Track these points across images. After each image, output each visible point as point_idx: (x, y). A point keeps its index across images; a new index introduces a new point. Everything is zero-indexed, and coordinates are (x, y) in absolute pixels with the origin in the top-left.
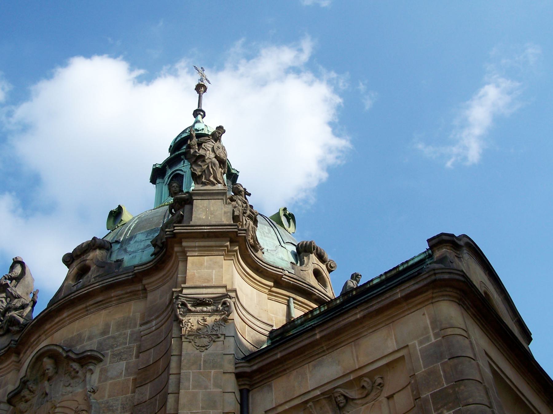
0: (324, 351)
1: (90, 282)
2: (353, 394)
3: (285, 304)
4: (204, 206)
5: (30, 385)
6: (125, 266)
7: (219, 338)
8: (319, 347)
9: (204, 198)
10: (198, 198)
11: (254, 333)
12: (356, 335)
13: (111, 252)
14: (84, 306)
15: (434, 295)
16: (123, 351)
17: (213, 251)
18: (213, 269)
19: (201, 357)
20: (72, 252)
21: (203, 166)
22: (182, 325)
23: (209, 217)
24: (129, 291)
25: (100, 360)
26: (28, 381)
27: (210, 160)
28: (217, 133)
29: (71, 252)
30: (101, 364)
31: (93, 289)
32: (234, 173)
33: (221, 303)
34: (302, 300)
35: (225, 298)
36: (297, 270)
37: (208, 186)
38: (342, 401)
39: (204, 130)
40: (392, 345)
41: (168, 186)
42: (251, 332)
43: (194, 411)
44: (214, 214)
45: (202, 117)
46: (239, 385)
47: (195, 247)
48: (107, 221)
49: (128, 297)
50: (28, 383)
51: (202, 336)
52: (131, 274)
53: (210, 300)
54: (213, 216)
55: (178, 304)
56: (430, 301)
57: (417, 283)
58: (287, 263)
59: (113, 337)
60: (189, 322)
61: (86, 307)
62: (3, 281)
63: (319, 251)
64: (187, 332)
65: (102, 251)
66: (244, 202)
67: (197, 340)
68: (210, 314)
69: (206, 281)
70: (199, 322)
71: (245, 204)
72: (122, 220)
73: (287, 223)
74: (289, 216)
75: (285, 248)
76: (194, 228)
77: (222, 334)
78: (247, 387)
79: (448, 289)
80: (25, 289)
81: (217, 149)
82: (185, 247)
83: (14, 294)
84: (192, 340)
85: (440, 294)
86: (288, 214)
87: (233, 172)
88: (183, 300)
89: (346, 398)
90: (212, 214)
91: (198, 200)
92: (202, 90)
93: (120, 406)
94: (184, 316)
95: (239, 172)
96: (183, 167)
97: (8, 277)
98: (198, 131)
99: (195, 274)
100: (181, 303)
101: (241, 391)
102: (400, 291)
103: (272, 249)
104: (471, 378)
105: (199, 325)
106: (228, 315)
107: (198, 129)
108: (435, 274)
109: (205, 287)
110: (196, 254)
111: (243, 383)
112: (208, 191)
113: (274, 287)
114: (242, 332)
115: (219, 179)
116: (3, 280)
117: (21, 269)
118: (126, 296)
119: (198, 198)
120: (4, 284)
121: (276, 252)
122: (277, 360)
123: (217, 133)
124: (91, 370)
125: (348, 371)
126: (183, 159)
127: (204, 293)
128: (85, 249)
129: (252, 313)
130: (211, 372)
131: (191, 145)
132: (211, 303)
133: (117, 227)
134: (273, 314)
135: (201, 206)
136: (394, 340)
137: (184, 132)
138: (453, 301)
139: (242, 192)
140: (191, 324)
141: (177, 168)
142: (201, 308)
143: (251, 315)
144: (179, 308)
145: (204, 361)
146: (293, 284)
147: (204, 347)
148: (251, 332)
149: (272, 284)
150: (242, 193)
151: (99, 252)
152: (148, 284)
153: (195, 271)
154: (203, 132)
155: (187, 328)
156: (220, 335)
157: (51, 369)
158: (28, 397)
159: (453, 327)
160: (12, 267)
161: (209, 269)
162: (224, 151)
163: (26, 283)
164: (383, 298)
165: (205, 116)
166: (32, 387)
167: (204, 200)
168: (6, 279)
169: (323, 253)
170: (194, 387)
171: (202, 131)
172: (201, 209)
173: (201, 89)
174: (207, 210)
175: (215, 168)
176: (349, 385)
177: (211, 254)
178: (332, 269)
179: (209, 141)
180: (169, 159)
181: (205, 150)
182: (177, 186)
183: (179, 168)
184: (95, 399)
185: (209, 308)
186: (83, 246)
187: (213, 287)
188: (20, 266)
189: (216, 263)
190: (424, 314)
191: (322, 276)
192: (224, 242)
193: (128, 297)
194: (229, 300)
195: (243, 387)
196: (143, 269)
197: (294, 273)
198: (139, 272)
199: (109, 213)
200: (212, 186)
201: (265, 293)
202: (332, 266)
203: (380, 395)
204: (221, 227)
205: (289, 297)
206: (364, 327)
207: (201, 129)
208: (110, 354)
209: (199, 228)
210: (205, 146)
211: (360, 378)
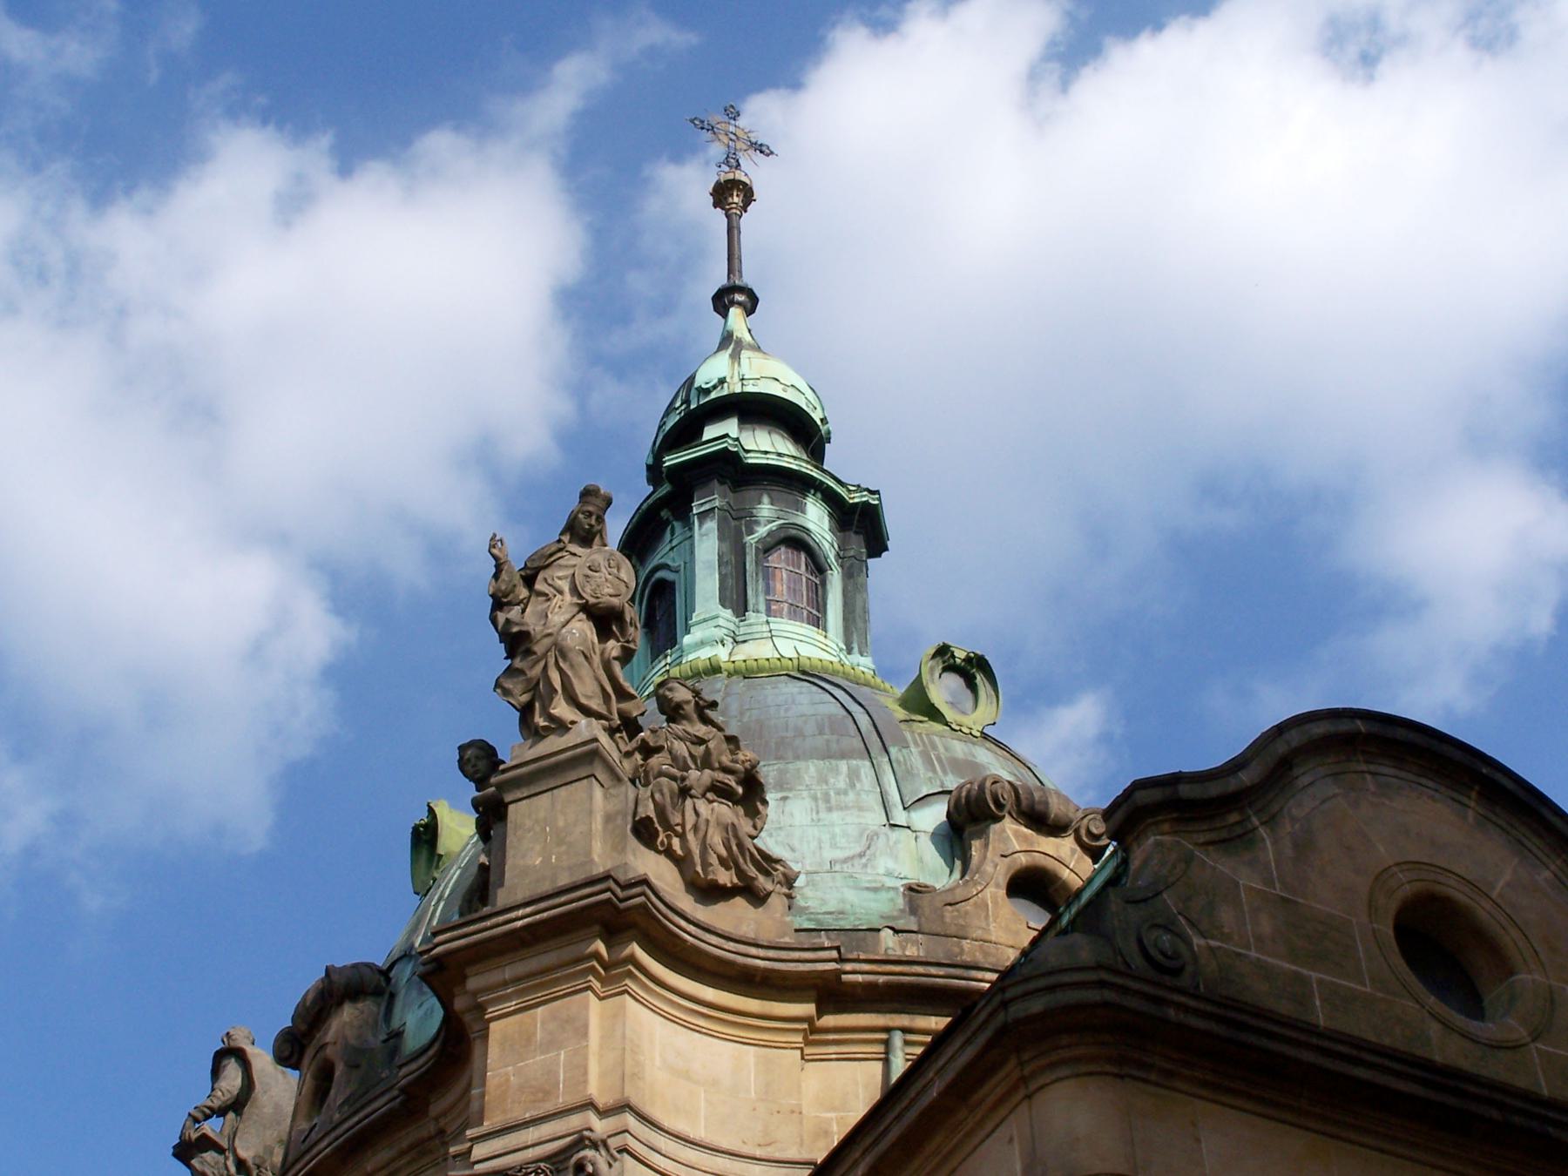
4: (537, 821)
6: (407, 1053)
9: (540, 790)
10: (519, 795)
13: (392, 996)
15: (1027, 1071)
17: (557, 982)
20: (292, 1022)
21: (528, 672)
23: (554, 857)
24: (405, 1144)
27: (547, 641)
28: (581, 516)
29: (290, 1025)
31: (316, 1159)
35: (578, 1152)
36: (927, 911)
39: (728, 380)
41: (644, 630)
44: (568, 839)
47: (505, 984)
48: (412, 864)
49: (409, 1163)
53: (540, 1168)
54: (564, 848)
56: (1022, 1092)
57: (968, 1042)
58: (891, 894)
63: (1024, 803)
65: (360, 1005)
66: (694, 739)
69: (540, 1095)
74: (969, 668)
75: (909, 827)
76: (488, 923)
79: (1065, 1040)
80: (268, 1133)
82: (475, 993)
85: (1043, 1062)
87: (856, 500)
90: (560, 842)
91: (520, 803)
95: (877, 492)
96: (671, 552)
98: (707, 392)
99: (508, 1080)
102: (936, 1074)
103: (847, 853)
107: (704, 386)
108: (1005, 1005)
110: (512, 1005)
112: (553, 760)
113: (821, 1012)
116: (190, 1128)
117: (240, 1074)
118: (402, 1162)
119: (519, 795)
121: (864, 860)
123: (581, 516)
126: (667, 522)
128: (316, 1010)
129: (725, 1145)
134: (834, 1109)
135: (528, 823)
137: (670, 409)
138: (1091, 1074)
143: (723, 1152)
146: (887, 985)
150: (683, 709)
151: (351, 1011)
152: (444, 1114)
153: (510, 1068)
154: (725, 392)
160: (216, 1072)
161: (548, 1052)
162: (618, 570)
163: (268, 1110)
164: (903, 1105)
168: (196, 1120)
169: (1040, 802)
171: (719, 388)
172: (529, 831)
173: (730, 200)
174: (548, 829)
175: (568, 663)
177: (552, 996)
178: (1098, 844)
179: (559, 555)
180: (629, 532)
181: (547, 595)
182: (477, 757)
183: (660, 561)
186: (308, 1004)
187: (554, 1114)
189: (567, 1021)
191: (1059, 883)
193: (409, 1163)
197: (915, 928)
198: (410, 1084)
199: (410, 836)
201: (792, 1048)
205: (888, 1030)
207: (715, 381)
209: (501, 919)
210: (545, 580)
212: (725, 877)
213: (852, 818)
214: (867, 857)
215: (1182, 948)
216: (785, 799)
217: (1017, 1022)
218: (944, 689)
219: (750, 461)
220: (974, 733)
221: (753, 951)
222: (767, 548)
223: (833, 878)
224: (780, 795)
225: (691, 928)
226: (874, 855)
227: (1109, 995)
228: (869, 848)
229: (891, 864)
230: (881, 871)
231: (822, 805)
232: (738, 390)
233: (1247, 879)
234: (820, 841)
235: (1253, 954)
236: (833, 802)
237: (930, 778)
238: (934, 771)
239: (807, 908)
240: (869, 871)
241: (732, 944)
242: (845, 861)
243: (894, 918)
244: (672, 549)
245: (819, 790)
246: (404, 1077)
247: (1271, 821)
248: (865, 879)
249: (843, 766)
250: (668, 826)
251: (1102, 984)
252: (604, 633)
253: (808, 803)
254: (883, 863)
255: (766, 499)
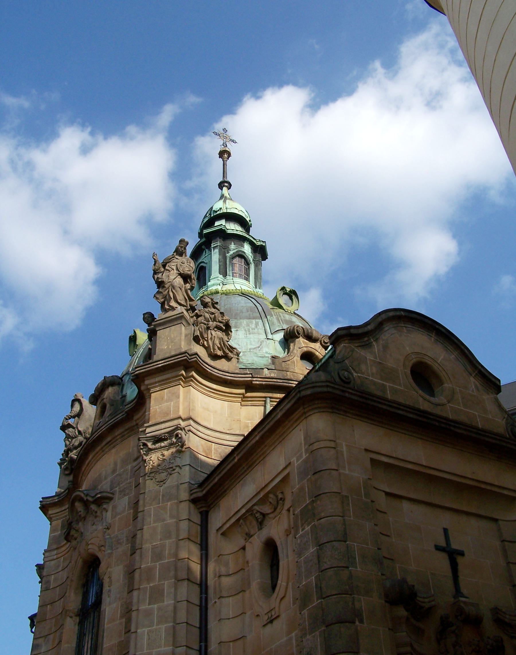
0: (246, 471)
1: (105, 420)
2: (266, 509)
3: (263, 406)
5: (74, 525)
7: (174, 470)
8: (241, 468)
9: (166, 327)
11: (223, 449)
12: (263, 454)
14: (99, 448)
15: (306, 410)
16: (125, 486)
18: (172, 401)
19: (160, 492)
20: (95, 392)
22: (146, 464)
25: (111, 499)
26: (72, 522)
27: (169, 284)
28: (179, 248)
30: (112, 502)
32: (259, 245)
33: (174, 436)
34: (279, 396)
37: (170, 312)
38: (259, 517)
39: (222, 208)
40: (282, 464)
42: (219, 448)
43: (154, 544)
45: (228, 188)
46: (199, 509)
47: (156, 383)
50: (73, 524)
51: (161, 471)
52: (124, 413)
54: (173, 344)
55: (140, 446)
57: (289, 402)
58: (267, 358)
59: (120, 475)
60: (150, 460)
61: (102, 448)
62: (65, 422)
63: (306, 333)
64: (150, 470)
65: (114, 388)
67: (157, 476)
68: (167, 448)
69: (166, 415)
70: (159, 458)
71: (213, 314)
72: (137, 345)
73: (290, 300)
75: (272, 339)
77: (176, 466)
78: (204, 509)
81: (181, 265)
82: (148, 385)
83: (71, 435)
84: (153, 477)
85: (310, 408)
86: (289, 291)
87: (259, 244)
88: (143, 441)
89: (262, 514)
90: (172, 342)
92: (226, 156)
93: (125, 538)
94: (147, 455)
97: (69, 417)
98: (216, 212)
100: (142, 444)
101: (201, 513)
103: (255, 347)
104: (327, 491)
105: (159, 461)
106: (182, 446)
107: (215, 210)
109: (164, 422)
110: (158, 389)
111: (200, 506)
112: (173, 317)
114: (206, 455)
115: (179, 301)
117: (79, 406)
120: (67, 424)
121: (259, 349)
122: (216, 483)
123: (179, 248)
124: (104, 509)
125: (259, 490)
126: (204, 249)
127: (162, 428)
130: (168, 504)
131: (156, 270)
132: (167, 438)
133: (134, 353)
136: (284, 458)
137: (205, 216)
138: (323, 412)
139: (209, 303)
140: (153, 461)
141: (200, 261)
142: (159, 444)
144: (142, 449)
145: (163, 495)
147: (162, 482)
148: (219, 448)
149: (243, 391)
150: (208, 304)
152: (138, 419)
153: (157, 407)
154: (221, 212)
155: (149, 466)
156: (174, 468)
157: (82, 511)
158: (76, 535)
159: (319, 441)
163: (87, 417)
165: (231, 185)
166: (76, 527)
167: (166, 329)
168: (67, 419)
170: (155, 522)
173: (224, 156)
174: (169, 338)
176: (264, 500)
179: (173, 259)
181: (169, 270)
184: (109, 535)
185: (166, 443)
188: (78, 404)
190: (301, 430)
192: (178, 372)
194: (179, 431)
195: (202, 510)
196: (130, 407)
197: (274, 369)
198: (128, 411)
200: (173, 311)
202: (326, 341)
203: (283, 509)
204: (173, 358)
205: (265, 397)
206: (266, 446)
207: (219, 209)
208: (118, 491)
210: (169, 266)
211: (266, 496)
212: (220, 353)
213: (256, 336)
214: (260, 348)
215: (350, 376)
216: (237, 330)
217: (304, 397)
218: (283, 300)
219: (228, 232)
220: (292, 312)
221: (227, 374)
222: (233, 257)
223: (251, 354)
224: (235, 329)
225: (210, 368)
226: (262, 347)
227: (329, 389)
228: (261, 345)
229: (267, 350)
230: (264, 352)
231: (248, 332)
232: (225, 211)
233: (369, 357)
234: (247, 343)
235: (371, 378)
236: (251, 332)
237: (279, 325)
238: (280, 323)
239: (243, 362)
240: (261, 351)
241: (221, 372)
242: (254, 349)
243: (268, 365)
244: (205, 257)
245: (247, 328)
246: (127, 408)
247: (376, 340)
248: (260, 354)
249: (254, 321)
250: (203, 338)
251: (327, 386)
252: (186, 282)
253: (244, 332)
254: (265, 350)
255: (233, 243)
